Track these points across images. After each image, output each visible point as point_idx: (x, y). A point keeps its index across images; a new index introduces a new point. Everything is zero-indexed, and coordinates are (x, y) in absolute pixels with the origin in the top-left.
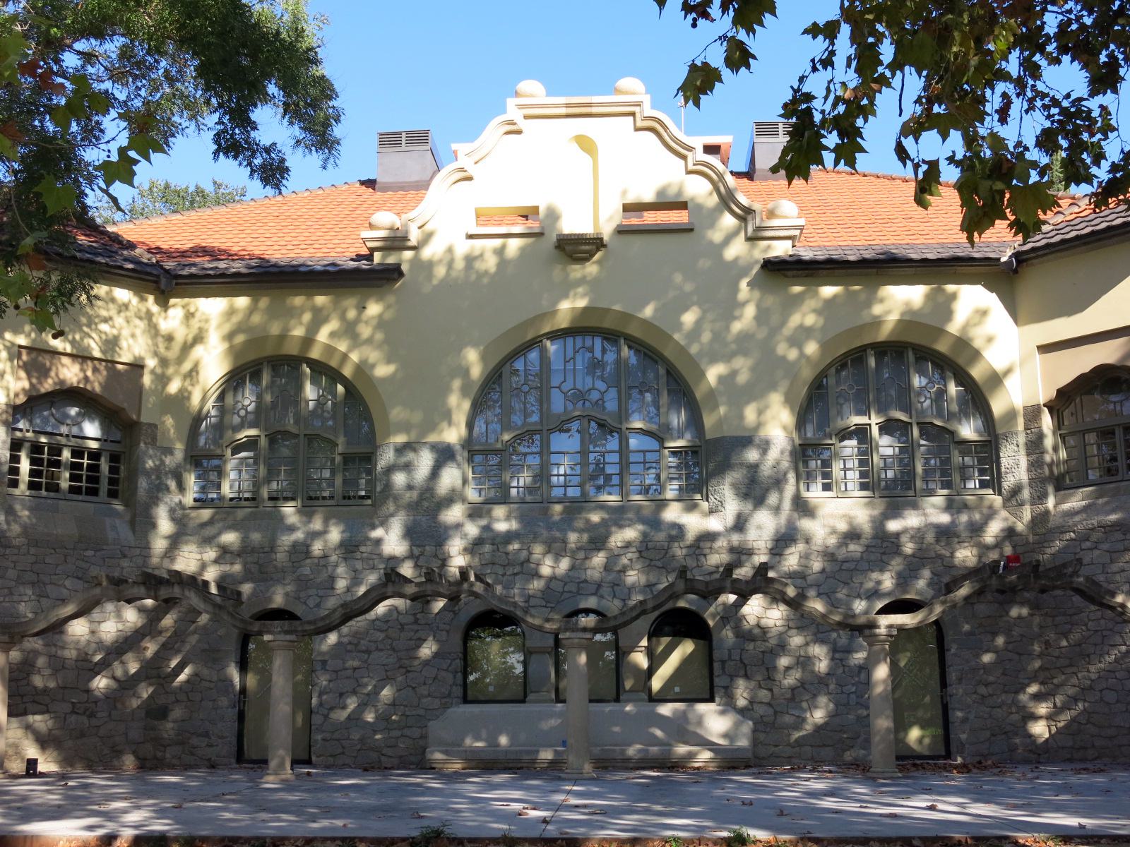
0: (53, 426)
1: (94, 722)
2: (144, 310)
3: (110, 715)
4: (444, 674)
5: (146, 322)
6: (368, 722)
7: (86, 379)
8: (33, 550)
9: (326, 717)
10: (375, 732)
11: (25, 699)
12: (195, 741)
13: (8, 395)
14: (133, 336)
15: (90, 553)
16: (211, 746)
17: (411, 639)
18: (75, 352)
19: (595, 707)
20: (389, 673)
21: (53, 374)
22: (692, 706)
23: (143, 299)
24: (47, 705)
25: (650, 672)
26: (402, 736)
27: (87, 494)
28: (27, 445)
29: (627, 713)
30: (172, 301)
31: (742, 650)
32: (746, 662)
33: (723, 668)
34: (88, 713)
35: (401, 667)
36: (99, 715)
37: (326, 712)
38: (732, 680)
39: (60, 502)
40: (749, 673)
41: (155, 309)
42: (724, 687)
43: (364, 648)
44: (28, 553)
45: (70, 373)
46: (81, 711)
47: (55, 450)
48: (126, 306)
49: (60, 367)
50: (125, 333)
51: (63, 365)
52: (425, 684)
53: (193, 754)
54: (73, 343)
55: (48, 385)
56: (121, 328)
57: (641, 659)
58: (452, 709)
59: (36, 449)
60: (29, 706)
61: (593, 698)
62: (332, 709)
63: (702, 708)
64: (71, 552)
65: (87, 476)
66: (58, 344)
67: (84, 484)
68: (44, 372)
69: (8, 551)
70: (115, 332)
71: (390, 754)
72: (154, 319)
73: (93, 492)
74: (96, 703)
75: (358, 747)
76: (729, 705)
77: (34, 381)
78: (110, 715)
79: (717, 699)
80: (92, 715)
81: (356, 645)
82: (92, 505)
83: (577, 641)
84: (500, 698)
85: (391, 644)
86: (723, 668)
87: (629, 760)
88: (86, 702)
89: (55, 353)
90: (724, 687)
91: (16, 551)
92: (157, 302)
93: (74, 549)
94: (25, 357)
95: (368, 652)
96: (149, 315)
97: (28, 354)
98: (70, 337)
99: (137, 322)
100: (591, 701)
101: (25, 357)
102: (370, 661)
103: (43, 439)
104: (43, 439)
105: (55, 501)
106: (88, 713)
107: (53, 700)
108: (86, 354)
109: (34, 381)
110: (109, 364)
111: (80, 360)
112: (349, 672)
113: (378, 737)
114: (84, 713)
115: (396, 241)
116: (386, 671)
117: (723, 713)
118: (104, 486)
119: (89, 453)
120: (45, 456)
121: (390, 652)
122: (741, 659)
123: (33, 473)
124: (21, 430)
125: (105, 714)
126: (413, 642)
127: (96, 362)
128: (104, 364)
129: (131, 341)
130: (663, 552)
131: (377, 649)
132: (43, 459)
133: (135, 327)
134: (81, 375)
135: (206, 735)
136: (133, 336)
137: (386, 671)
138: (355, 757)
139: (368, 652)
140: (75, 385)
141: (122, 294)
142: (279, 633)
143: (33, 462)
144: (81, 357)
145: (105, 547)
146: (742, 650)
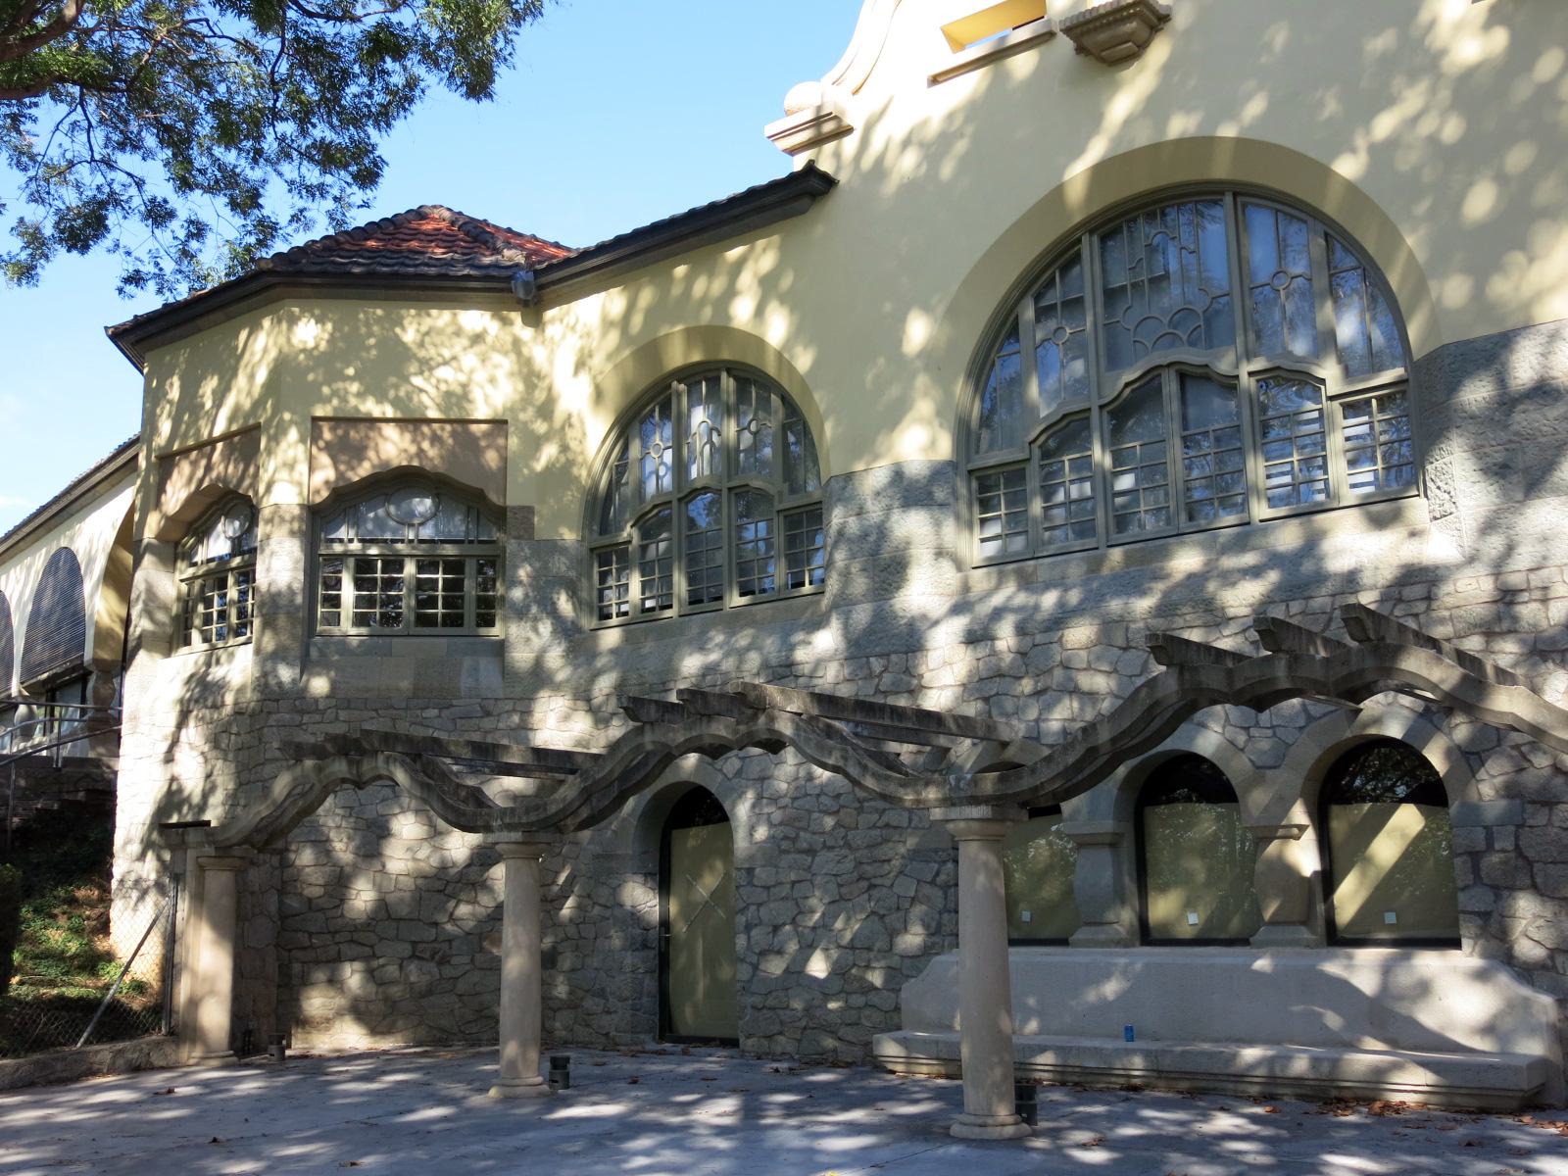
0: (394, 532)
1: (448, 971)
2: (509, 339)
3: (472, 961)
4: (927, 890)
5: (513, 357)
6: (815, 979)
7: (421, 452)
8: (343, 715)
9: (756, 967)
10: (827, 997)
11: (338, 938)
12: (589, 1003)
13: (301, 493)
14: (492, 380)
15: (432, 713)
16: (609, 1012)
17: (874, 827)
18: (399, 415)
19: (1017, 954)
20: (844, 890)
21: (371, 454)
22: (1407, 957)
23: (506, 322)
24: (372, 947)
25: (1328, 879)
26: (867, 1005)
27: (444, 624)
28: (351, 562)
29: (1260, 974)
30: (549, 314)
31: (1520, 826)
32: (1530, 854)
33: (1476, 870)
34: (437, 957)
35: (860, 878)
36: (455, 960)
37: (755, 959)
38: (1498, 897)
39: (395, 640)
40: (1539, 880)
41: (526, 333)
42: (1478, 914)
43: (805, 845)
44: (337, 718)
45: (393, 447)
46: (427, 955)
47: (394, 563)
48: (477, 339)
49: (380, 441)
50: (480, 376)
51: (385, 439)
52: (898, 909)
53: (588, 1026)
54: (396, 403)
55: (364, 470)
56: (472, 372)
57: (1305, 857)
58: (938, 958)
59: (364, 565)
60: (344, 948)
61: (1015, 935)
62: (763, 953)
63: (1428, 962)
64: (402, 713)
65: (444, 597)
66: (371, 407)
67: (440, 610)
68: (358, 452)
69: (306, 718)
70: (462, 378)
71: (849, 1038)
72: (525, 351)
73: (454, 620)
74: (450, 941)
75: (803, 1023)
76: (1502, 956)
77: (342, 467)
78: (472, 961)
79: (1465, 942)
80: (444, 961)
81: (794, 840)
82: (444, 640)
83: (962, 825)
84: (1045, 934)
85: (844, 837)
86: (1476, 870)
87: (1240, 1077)
88: (435, 941)
89: (372, 422)
90: (1478, 914)
91: (318, 717)
92: (526, 322)
93: (406, 709)
94: (327, 435)
95: (811, 852)
96: (517, 344)
97: (333, 430)
98: (392, 394)
99: (497, 358)
100: (1013, 942)
101: (327, 435)
102: (814, 867)
103: (374, 551)
104: (374, 551)
105: (387, 640)
106: (437, 957)
107: (381, 939)
108: (417, 416)
109: (342, 467)
110: (459, 428)
111: (411, 427)
112: (785, 890)
113: (832, 1005)
114: (432, 958)
115: (826, 129)
116: (840, 886)
117: (1481, 976)
118: (470, 611)
119: (444, 562)
120: (379, 575)
121: (844, 851)
122: (1517, 847)
123: (359, 601)
124: (341, 541)
125: (466, 959)
126: (877, 832)
127: (436, 426)
128: (448, 427)
129: (488, 388)
130: (1325, 617)
131: (825, 846)
132: (376, 579)
133: (496, 367)
134: (413, 449)
135: (601, 993)
136: (492, 380)
137: (840, 886)
138: (799, 1041)
139: (811, 852)
140: (404, 463)
141: (475, 319)
142: (501, 829)
143: (359, 584)
144: (411, 422)
145: (454, 702)
146: (1520, 826)
